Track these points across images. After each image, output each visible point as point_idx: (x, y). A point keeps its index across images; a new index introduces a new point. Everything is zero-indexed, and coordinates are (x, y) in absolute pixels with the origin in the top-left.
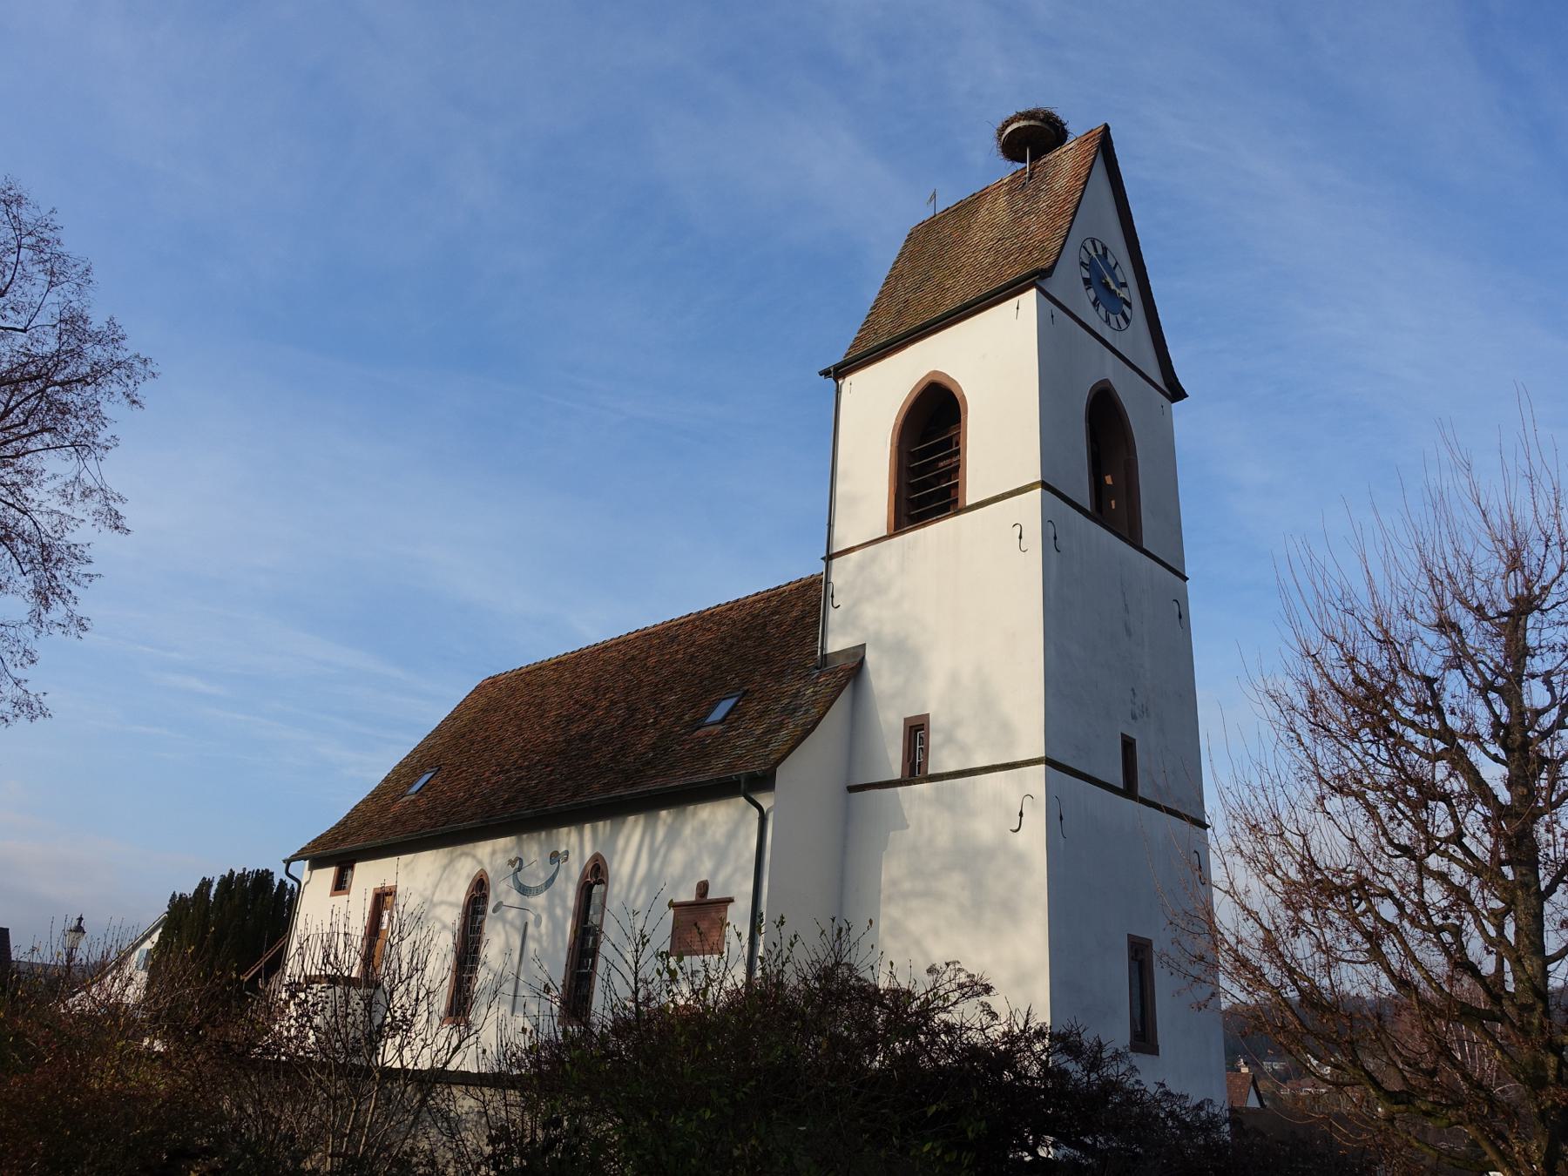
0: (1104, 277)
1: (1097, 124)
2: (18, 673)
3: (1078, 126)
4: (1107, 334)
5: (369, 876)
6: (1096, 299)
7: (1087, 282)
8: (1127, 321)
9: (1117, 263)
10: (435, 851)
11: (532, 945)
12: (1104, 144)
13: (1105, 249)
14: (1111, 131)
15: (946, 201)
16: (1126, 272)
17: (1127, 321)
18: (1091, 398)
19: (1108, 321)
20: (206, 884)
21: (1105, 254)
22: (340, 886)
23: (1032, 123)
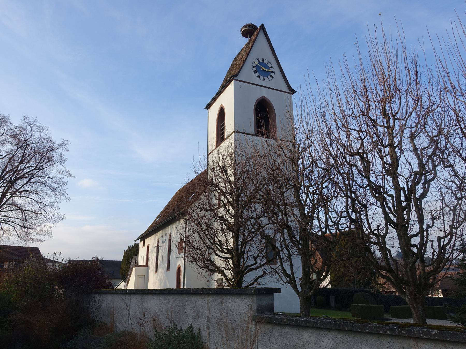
0: (261, 68)
1: (260, 25)
2: (57, 212)
3: (258, 26)
4: (264, 84)
5: (148, 241)
6: (259, 75)
8: (272, 77)
9: (268, 62)
10: (154, 235)
11: (164, 254)
12: (262, 27)
13: (263, 60)
15: (238, 52)
16: (273, 62)
17: (272, 77)
18: (256, 103)
19: (264, 80)
20: (129, 247)
21: (263, 61)
22: (144, 245)
23: (246, 28)
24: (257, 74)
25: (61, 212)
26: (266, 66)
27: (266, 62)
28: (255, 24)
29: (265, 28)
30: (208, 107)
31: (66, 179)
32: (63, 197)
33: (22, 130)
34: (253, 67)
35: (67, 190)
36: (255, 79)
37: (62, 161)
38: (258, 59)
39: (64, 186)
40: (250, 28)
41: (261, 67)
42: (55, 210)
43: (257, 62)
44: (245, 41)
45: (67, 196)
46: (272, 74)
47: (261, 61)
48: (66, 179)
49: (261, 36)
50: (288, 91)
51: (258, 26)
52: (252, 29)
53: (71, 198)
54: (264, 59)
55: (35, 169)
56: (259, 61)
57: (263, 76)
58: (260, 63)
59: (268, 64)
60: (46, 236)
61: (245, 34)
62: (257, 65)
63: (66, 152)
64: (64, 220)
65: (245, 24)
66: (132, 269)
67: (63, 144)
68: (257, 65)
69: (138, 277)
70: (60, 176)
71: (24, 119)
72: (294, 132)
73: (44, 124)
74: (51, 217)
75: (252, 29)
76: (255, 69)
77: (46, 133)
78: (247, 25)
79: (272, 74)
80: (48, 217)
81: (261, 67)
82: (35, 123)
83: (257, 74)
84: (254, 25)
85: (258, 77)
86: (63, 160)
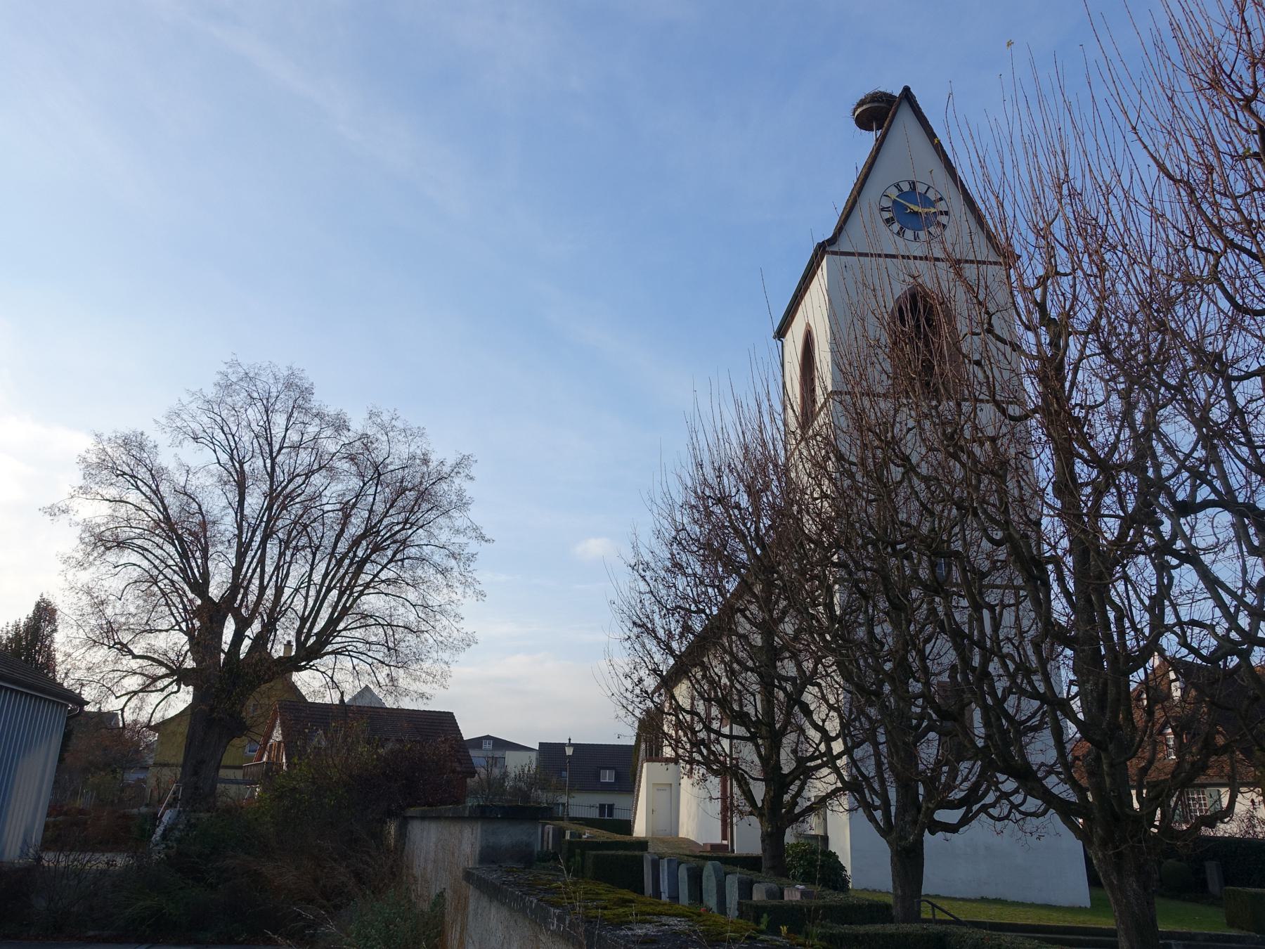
0: (906, 208)
2: (458, 626)
3: (897, 93)
6: (901, 228)
7: (889, 221)
14: (912, 90)
23: (865, 107)
24: (896, 227)
25: (467, 626)
26: (927, 202)
27: (921, 188)
28: (889, 91)
29: (913, 97)
30: (781, 333)
31: (473, 546)
32: (469, 592)
33: (366, 441)
34: (883, 209)
35: (474, 572)
36: (889, 240)
37: (462, 504)
38: (897, 186)
39: (471, 564)
40: (876, 104)
41: (907, 204)
42: (454, 623)
43: (894, 193)
44: (869, 139)
45: (478, 587)
46: (943, 219)
47: (906, 188)
48: (473, 546)
49: (904, 118)
50: (993, 257)
51: (897, 93)
52: (882, 105)
53: (486, 591)
54: (914, 183)
55: (403, 529)
56: (900, 190)
57: (915, 230)
58: (902, 194)
59: (927, 195)
60: (434, 685)
61: (864, 121)
62: (894, 202)
63: (469, 482)
64: (474, 645)
65: (869, 90)
66: (642, 767)
67: (461, 464)
68: (894, 202)
69: (655, 787)
70: (460, 539)
71: (370, 418)
72: (814, 401)
73: (414, 423)
74: (445, 638)
75: (882, 105)
76: (887, 215)
77: (420, 443)
78: (866, 98)
79: (943, 219)
80: (440, 639)
81: (907, 204)
82: (394, 422)
83: (896, 227)
84: (885, 94)
85: (898, 233)
86: (464, 501)
